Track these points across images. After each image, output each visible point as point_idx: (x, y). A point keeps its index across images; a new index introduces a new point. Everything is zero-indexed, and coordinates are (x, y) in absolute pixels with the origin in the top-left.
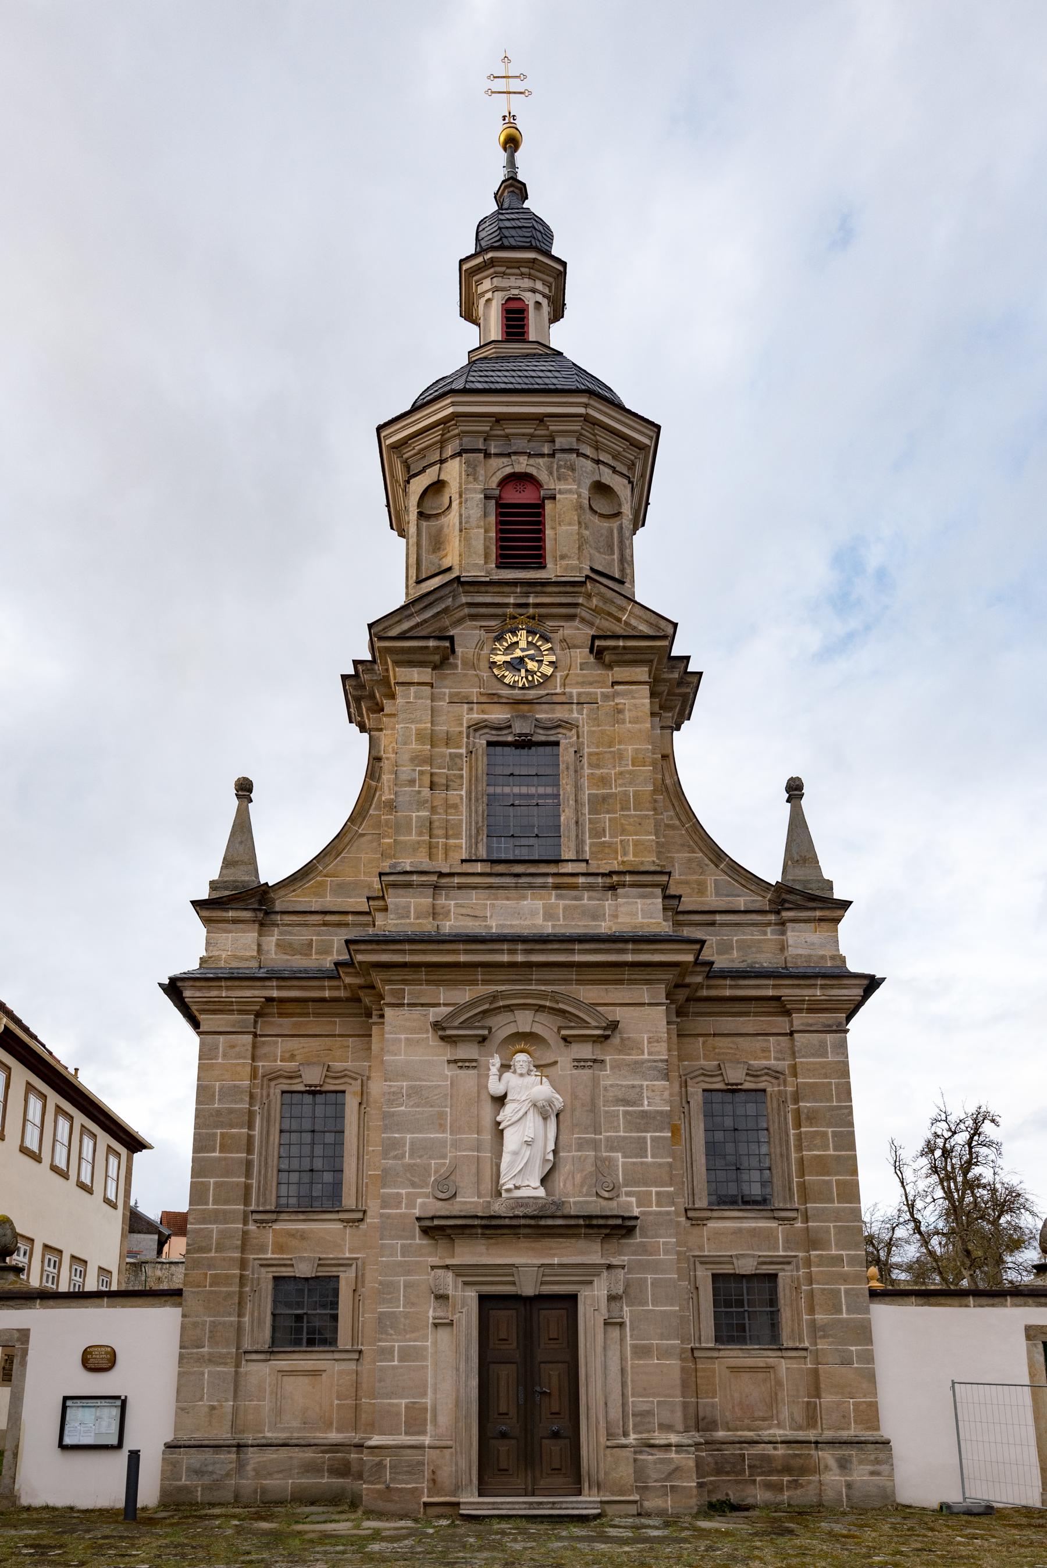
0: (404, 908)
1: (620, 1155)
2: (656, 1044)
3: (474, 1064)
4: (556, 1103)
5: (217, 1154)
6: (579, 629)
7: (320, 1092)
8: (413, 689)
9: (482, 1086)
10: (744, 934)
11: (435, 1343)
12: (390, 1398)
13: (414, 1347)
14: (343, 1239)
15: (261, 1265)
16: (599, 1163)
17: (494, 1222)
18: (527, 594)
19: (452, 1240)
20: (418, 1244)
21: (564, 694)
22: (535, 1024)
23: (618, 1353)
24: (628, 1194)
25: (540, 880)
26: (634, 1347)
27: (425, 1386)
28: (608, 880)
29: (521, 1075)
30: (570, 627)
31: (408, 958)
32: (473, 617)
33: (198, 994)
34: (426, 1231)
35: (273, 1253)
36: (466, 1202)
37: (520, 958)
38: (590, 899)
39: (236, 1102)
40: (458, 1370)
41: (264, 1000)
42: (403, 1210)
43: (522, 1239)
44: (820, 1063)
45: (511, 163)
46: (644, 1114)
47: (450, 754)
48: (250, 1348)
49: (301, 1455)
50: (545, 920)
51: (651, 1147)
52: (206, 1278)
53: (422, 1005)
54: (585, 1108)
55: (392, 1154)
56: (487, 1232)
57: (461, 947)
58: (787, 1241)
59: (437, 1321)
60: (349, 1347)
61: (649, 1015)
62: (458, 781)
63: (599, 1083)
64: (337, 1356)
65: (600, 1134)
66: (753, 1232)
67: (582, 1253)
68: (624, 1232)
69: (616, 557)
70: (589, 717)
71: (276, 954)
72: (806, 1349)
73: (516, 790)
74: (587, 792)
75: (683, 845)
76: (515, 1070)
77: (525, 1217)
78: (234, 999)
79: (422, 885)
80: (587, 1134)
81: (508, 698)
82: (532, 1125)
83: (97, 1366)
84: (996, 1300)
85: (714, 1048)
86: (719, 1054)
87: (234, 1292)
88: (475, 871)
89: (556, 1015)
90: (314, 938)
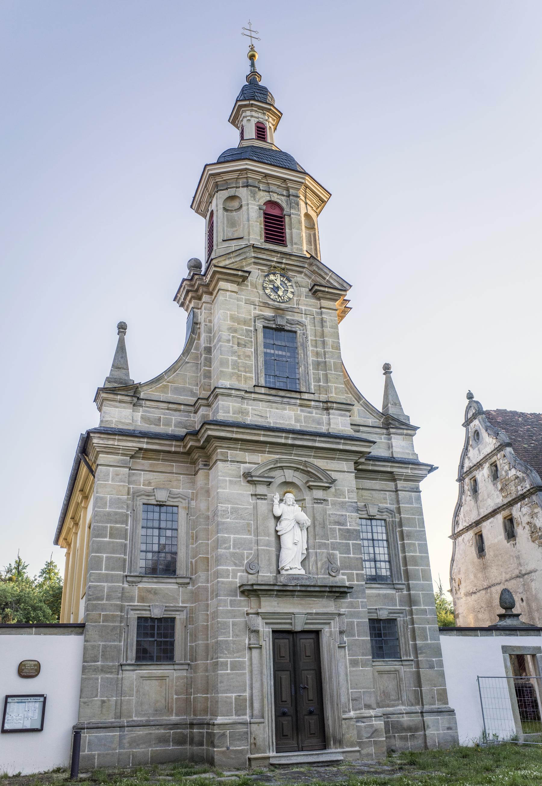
1: (338, 552)
2: (351, 493)
5: (107, 539)
6: (304, 279)
7: (164, 505)
8: (228, 293)
12: (227, 693)
13: (238, 661)
14: (178, 595)
15: (132, 610)
18: (282, 258)
20: (239, 600)
24: (343, 574)
25: (293, 401)
26: (351, 660)
28: (325, 405)
30: (300, 277)
31: (235, 436)
33: (101, 442)
34: (243, 592)
35: (138, 602)
36: (264, 576)
37: (290, 442)
38: (316, 413)
39: (119, 508)
41: (138, 449)
42: (230, 580)
44: (410, 507)
46: (348, 531)
49: (157, 731)
51: (353, 549)
52: (100, 617)
53: (238, 462)
57: (262, 433)
60: (183, 662)
62: (250, 343)
64: (176, 667)
66: (385, 595)
67: (325, 607)
71: (141, 422)
72: (412, 660)
73: (276, 352)
74: (311, 359)
78: (121, 447)
80: (323, 540)
81: (273, 306)
83: (28, 674)
85: (362, 496)
86: (365, 499)
88: (261, 392)
89: (304, 474)
90: (162, 416)
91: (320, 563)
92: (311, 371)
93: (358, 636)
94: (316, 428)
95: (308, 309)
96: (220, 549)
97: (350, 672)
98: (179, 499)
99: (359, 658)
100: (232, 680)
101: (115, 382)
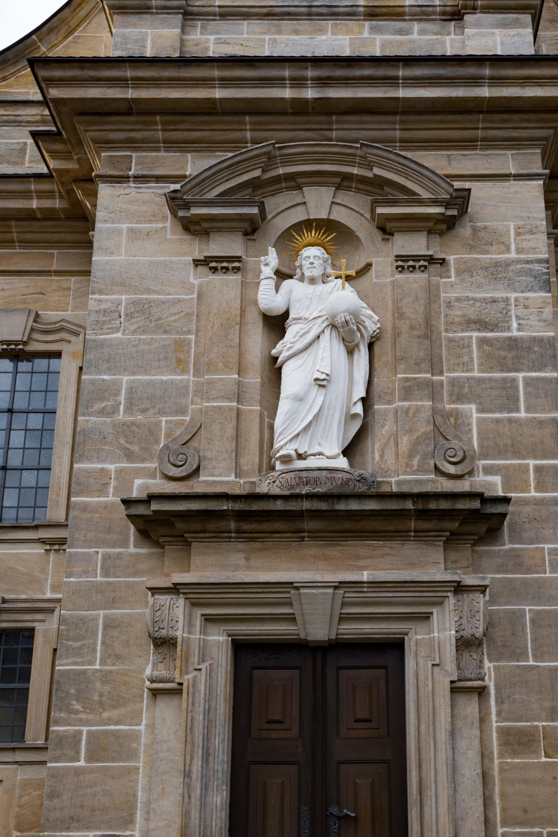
0: (136, 41)
1: (473, 407)
2: (528, 237)
3: (236, 264)
4: (368, 323)
11: (151, 727)
13: (116, 734)
14: (44, 571)
16: (439, 419)
17: (256, 506)
19: (189, 544)
20: (131, 555)
22: (335, 208)
23: (476, 743)
24: (488, 470)
26: (504, 733)
27: (132, 807)
29: (312, 281)
38: (422, 32)
40: (187, 774)
43: (307, 542)
51: (525, 394)
54: (416, 333)
55: (98, 406)
56: (246, 527)
59: (155, 685)
61: (517, 192)
63: (438, 296)
64: (20, 757)
65: (441, 373)
67: (412, 565)
68: (483, 528)
76: (303, 274)
77: (310, 496)
80: (420, 372)
82: (327, 354)
91: (405, 439)
93: (534, 656)
96: (84, 415)
97: (501, 770)
98: (63, 335)
99: (537, 727)
100: (88, 791)
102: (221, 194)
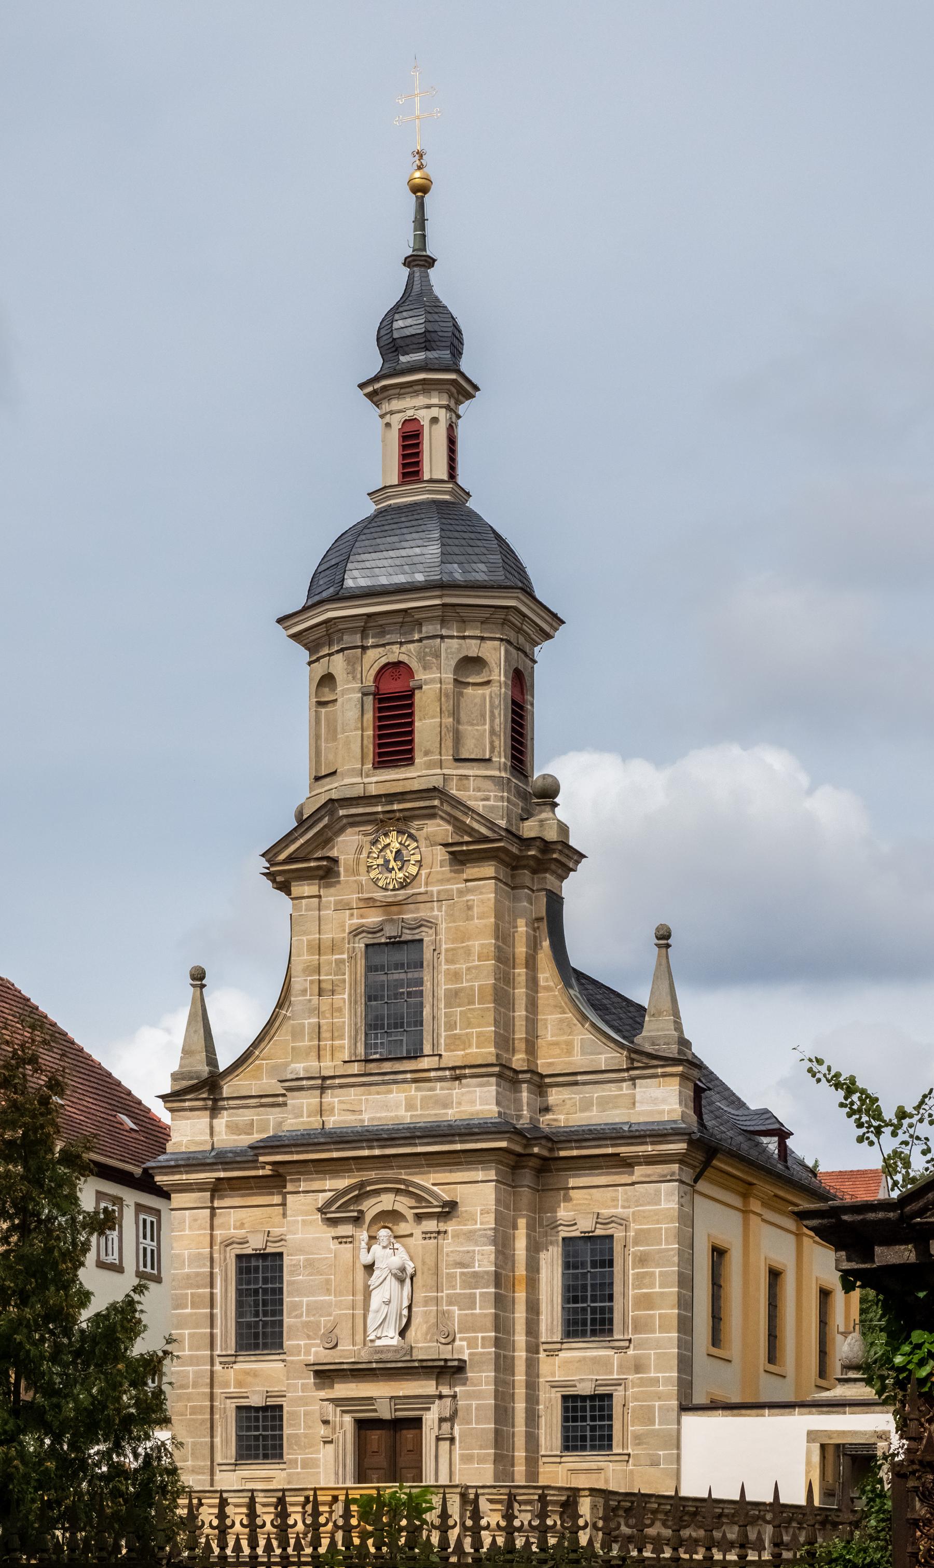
1: (456, 1308)
3: (350, 1240)
5: (188, 1311)
6: (439, 825)
9: (355, 1257)
10: (604, 1090)
13: (311, 1459)
15: (227, 1398)
18: (391, 803)
21: (426, 893)
24: (462, 1339)
32: (352, 825)
37: (377, 1152)
38: (442, 1089)
44: (654, 1210)
45: (420, 221)
46: (475, 1275)
47: (336, 960)
48: (221, 1462)
50: (407, 1111)
53: (313, 1191)
55: (294, 1314)
57: (332, 1147)
58: (620, 1366)
63: (442, 1251)
65: (442, 1292)
66: (594, 1360)
67: (422, 1387)
69: (487, 727)
70: (447, 914)
75: (555, 1006)
79: (311, 1088)
84: (787, 1410)
87: (206, 1419)
90: (255, 1118)
92: (443, 1010)
94: (436, 1115)
95: (443, 890)
101: (183, 1079)
102: (338, 1208)
